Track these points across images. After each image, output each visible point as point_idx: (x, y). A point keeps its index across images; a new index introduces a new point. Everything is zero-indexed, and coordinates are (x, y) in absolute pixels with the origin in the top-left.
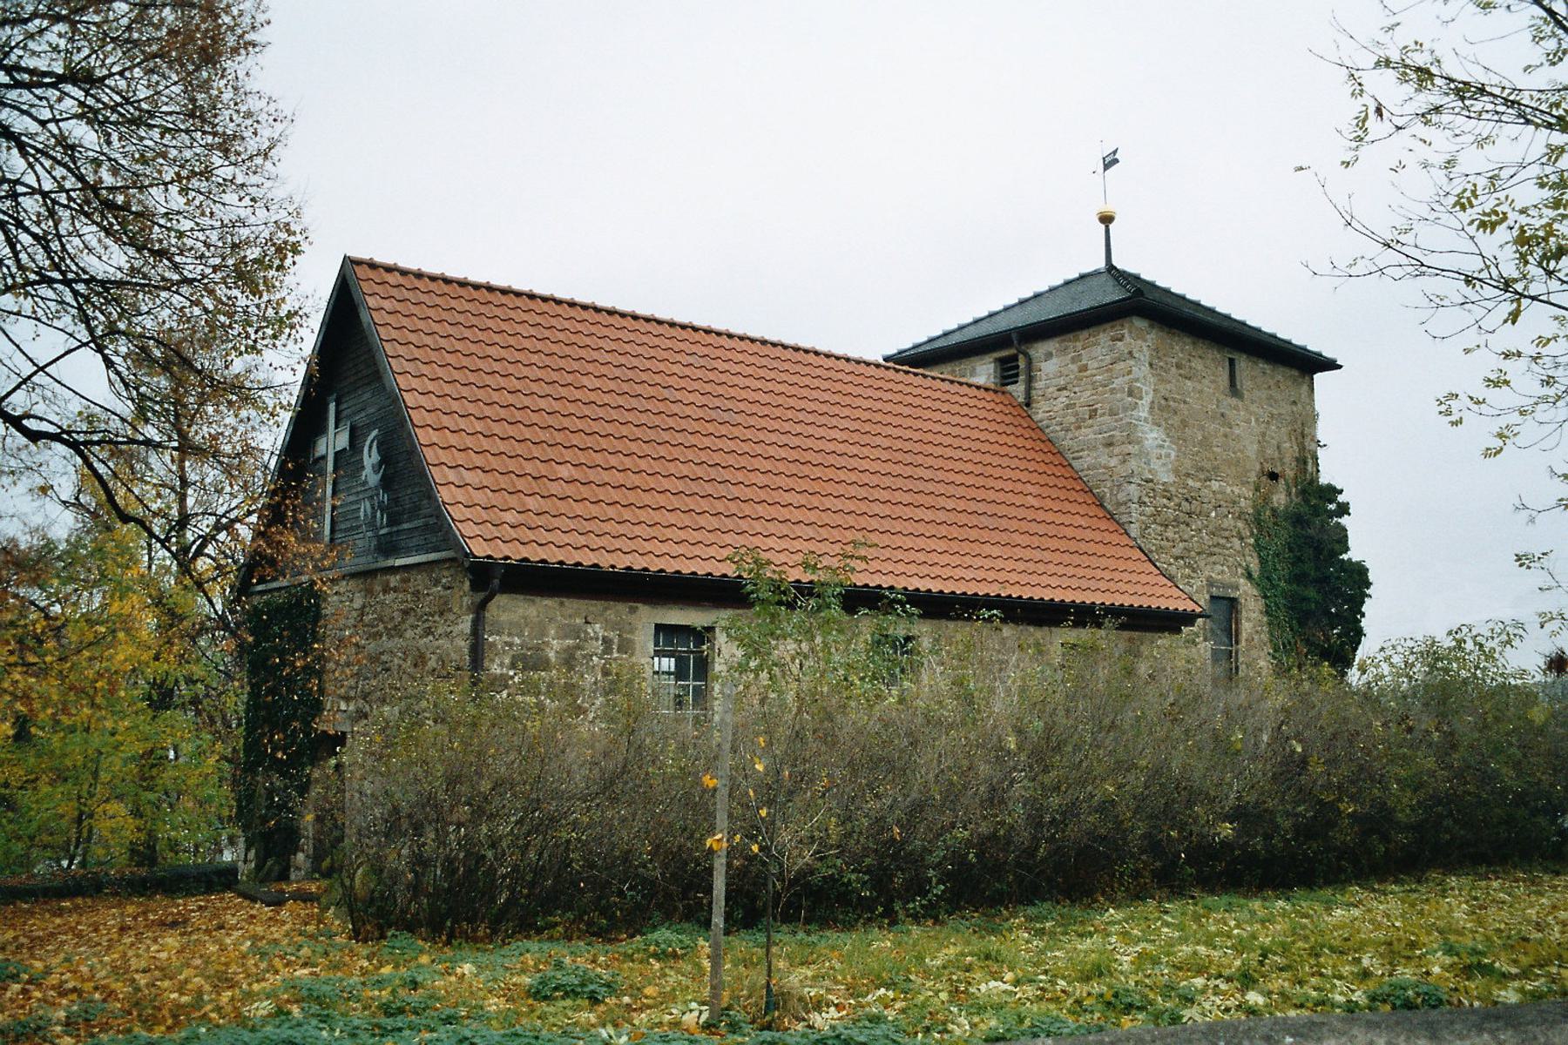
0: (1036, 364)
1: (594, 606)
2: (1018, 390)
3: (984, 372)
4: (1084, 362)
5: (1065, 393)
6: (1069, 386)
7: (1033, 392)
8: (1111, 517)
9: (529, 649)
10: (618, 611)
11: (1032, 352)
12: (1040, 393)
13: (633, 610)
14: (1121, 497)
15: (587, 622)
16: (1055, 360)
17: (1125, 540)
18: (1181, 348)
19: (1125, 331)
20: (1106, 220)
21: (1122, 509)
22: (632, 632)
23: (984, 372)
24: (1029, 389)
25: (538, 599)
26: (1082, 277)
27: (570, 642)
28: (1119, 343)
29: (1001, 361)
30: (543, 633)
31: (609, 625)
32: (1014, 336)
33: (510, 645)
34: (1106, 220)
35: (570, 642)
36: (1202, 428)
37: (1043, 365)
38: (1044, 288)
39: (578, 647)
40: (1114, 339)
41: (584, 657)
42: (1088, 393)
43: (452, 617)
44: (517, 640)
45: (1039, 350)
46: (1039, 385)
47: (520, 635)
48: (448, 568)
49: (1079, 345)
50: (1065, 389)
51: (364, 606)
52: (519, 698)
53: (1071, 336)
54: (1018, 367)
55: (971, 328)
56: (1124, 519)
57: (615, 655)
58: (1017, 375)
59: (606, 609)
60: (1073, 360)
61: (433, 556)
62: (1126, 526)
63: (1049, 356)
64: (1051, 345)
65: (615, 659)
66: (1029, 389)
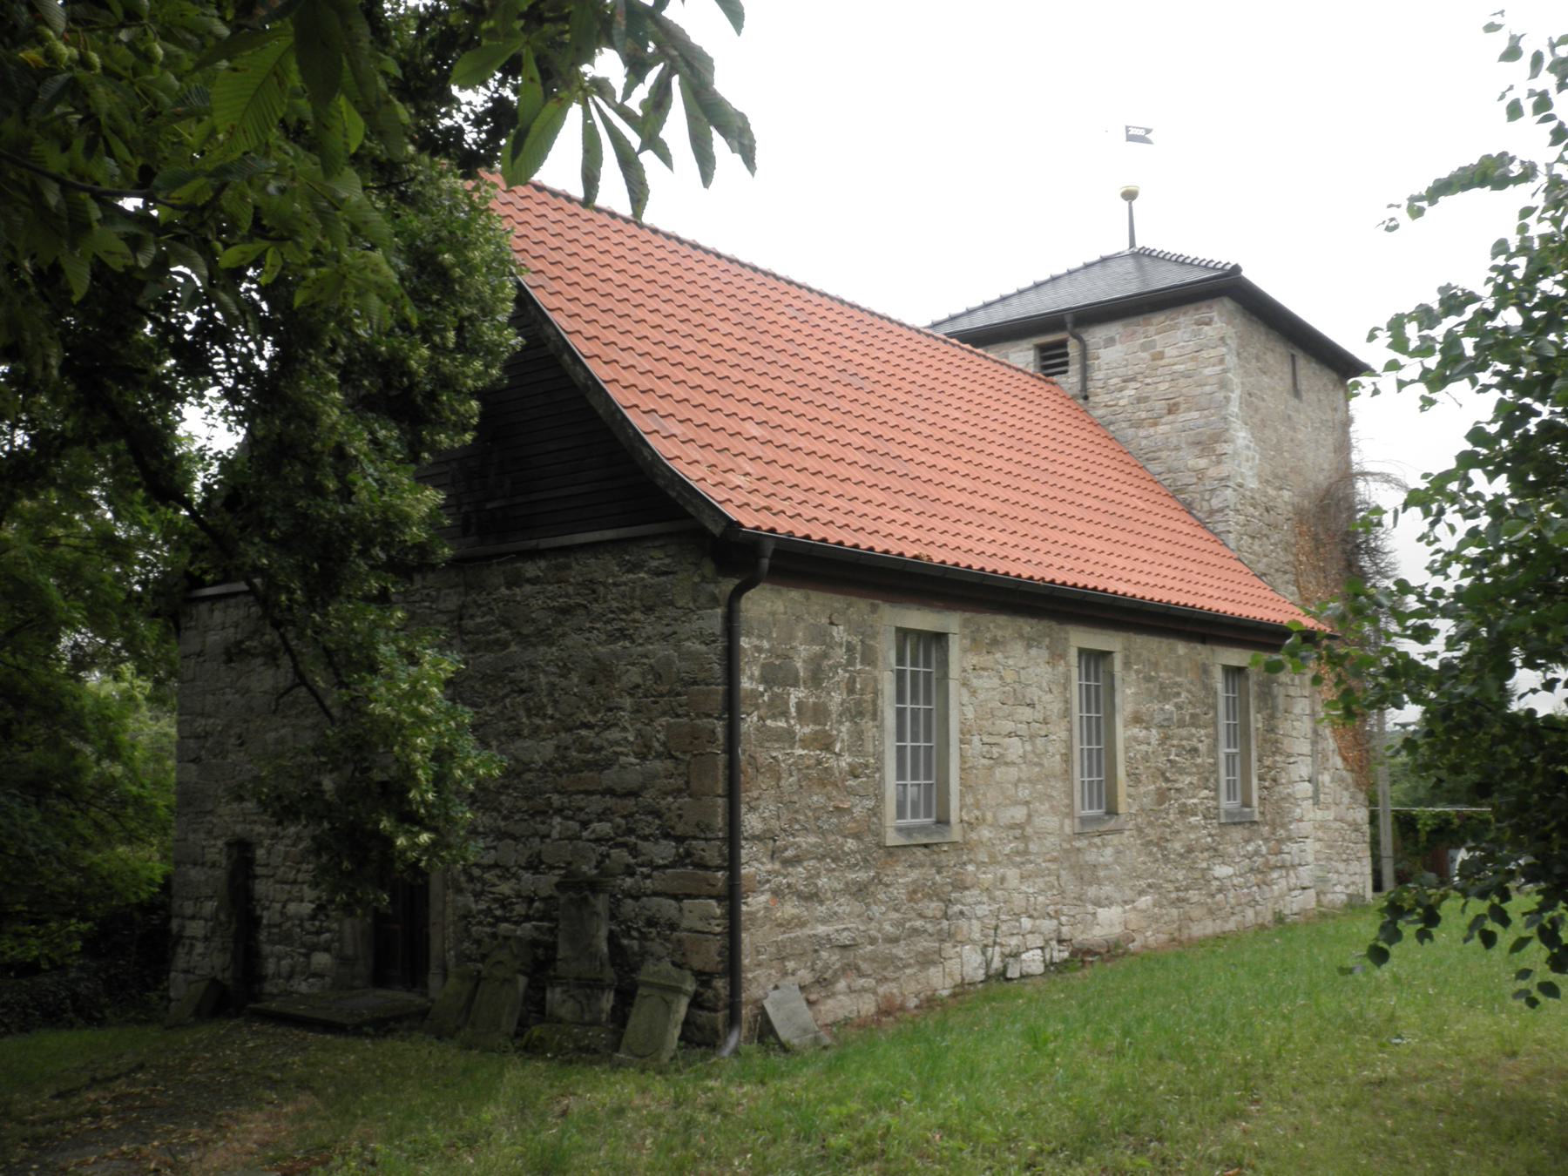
0: (1091, 351)
1: (837, 601)
2: (1070, 380)
3: (1023, 355)
4: (1158, 349)
5: (1133, 385)
6: (1140, 377)
7: (1090, 384)
8: (1203, 525)
9: (778, 657)
10: (859, 608)
11: (1085, 337)
12: (1100, 384)
13: (874, 609)
14: (1216, 503)
15: (832, 623)
16: (1118, 347)
17: (1223, 550)
18: (1260, 339)
19: (1215, 314)
20: (1130, 196)
21: (1218, 517)
22: (874, 636)
23: (1023, 355)
24: (1085, 379)
25: (784, 590)
26: (1104, 260)
27: (816, 649)
28: (1206, 328)
29: (1042, 349)
30: (792, 637)
31: (853, 628)
32: (1068, 318)
33: (759, 649)
34: (1130, 196)
35: (816, 649)
36: (1276, 430)
37: (1102, 352)
38: (1062, 271)
39: (825, 656)
40: (1199, 323)
41: (830, 667)
42: (1167, 385)
43: (670, 612)
44: (766, 645)
45: (1096, 336)
46: (1098, 375)
47: (769, 638)
48: (662, 547)
49: (1152, 329)
50: (1133, 379)
51: (463, 606)
52: (769, 722)
53: (1140, 319)
54: (1066, 355)
55: (981, 313)
56: (1221, 527)
57: (859, 667)
58: (1066, 364)
59: (850, 605)
60: (1144, 348)
61: (609, 534)
62: (1223, 536)
63: (1110, 342)
64: (1114, 329)
65: (859, 672)
66: (1085, 379)
